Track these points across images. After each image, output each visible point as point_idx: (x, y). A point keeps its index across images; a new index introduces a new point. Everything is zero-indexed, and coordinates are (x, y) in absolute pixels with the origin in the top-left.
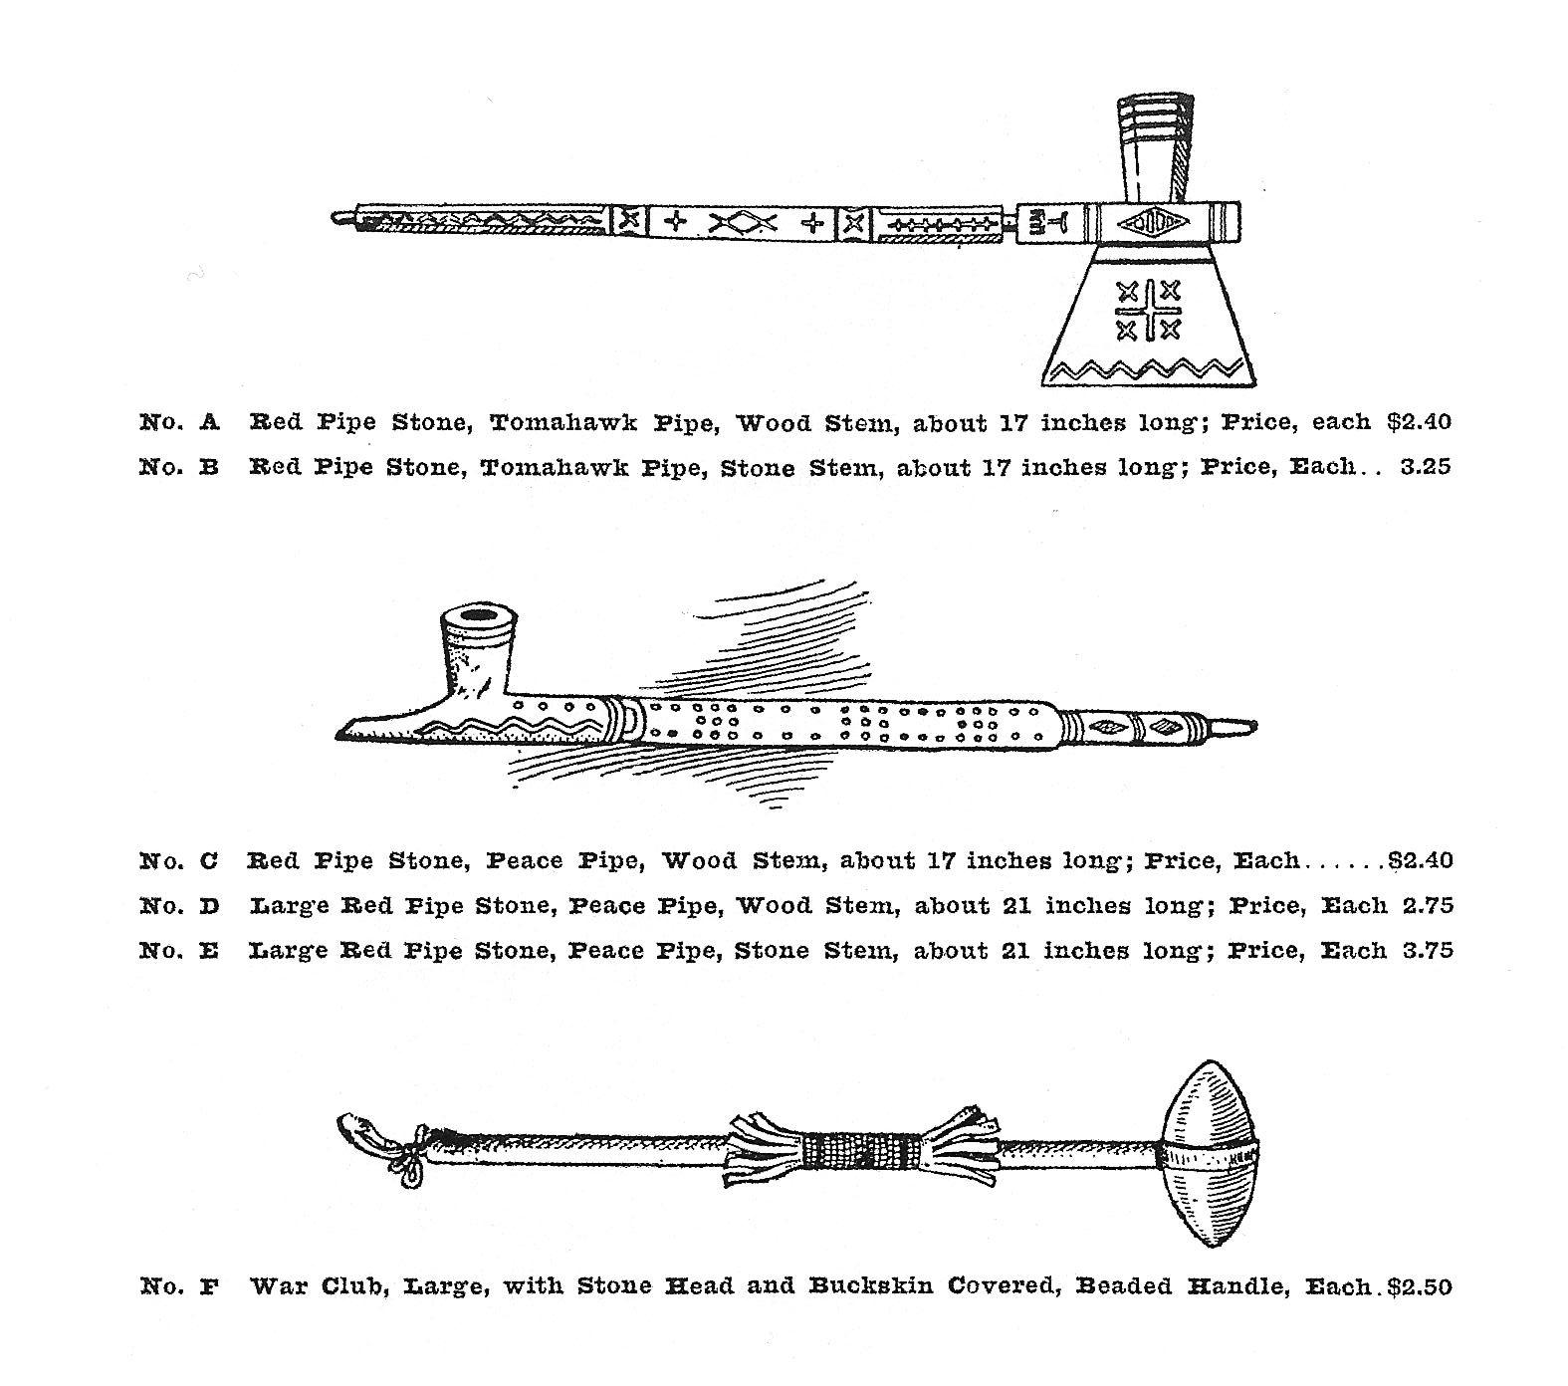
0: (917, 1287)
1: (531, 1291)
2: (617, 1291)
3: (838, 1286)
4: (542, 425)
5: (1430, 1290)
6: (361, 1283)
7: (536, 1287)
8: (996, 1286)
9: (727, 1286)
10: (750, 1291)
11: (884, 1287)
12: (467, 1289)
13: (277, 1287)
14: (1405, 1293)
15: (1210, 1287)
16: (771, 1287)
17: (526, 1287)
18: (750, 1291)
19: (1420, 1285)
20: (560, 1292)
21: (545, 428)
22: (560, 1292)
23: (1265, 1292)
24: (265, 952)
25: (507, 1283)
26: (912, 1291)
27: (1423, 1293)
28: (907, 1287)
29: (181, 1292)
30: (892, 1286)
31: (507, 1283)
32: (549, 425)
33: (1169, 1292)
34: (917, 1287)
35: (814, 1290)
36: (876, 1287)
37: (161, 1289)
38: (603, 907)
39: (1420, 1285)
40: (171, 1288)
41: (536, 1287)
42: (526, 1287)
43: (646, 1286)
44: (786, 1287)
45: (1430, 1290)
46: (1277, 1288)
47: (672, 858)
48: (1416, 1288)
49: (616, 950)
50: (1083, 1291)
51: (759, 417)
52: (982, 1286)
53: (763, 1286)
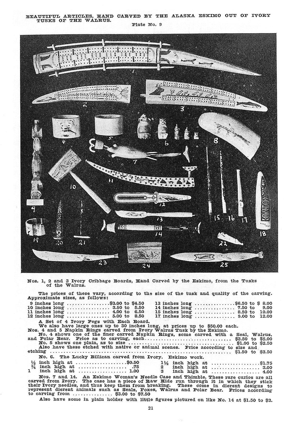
0: (180, 358)
1: (107, 348)
2: (218, 15)
3: (103, 390)
4: (87, 390)
5: (268, 352)
6: (197, 377)
7: (132, 400)
8: (205, 335)
9: (208, 294)
10: (230, 336)
11: (197, 281)
12: (108, 281)
13: (257, 335)
14: (263, 344)
15: (140, 281)
16: (204, 294)
17: (130, 400)
18: (201, 348)
19: (266, 352)
20: (65, 372)
21: (88, 391)
22: (65, 372)
23: (95, 299)
24: (98, 21)
25: (191, 357)
26: (179, 358)
27: (256, 303)
28: (102, 377)
29: (85, 286)
30: (199, 281)
31: (191, 357)
32: (88, 390)
33: (149, 282)
34: (204, 281)
35: (92, 358)
36: (254, 281)
37: (31, 281)
38: (228, 326)
39: (266, 352)
40: (224, 400)
41: (132, 400)
42: (130, 400)
43: (214, 400)
44: (180, 377)
45: (243, 352)
46: (130, 281)
47: (116, 376)
48: (265, 343)
49: (231, 326)
50: (145, 17)
51: (119, 376)
52: (64, 334)
53: (176, 377)
